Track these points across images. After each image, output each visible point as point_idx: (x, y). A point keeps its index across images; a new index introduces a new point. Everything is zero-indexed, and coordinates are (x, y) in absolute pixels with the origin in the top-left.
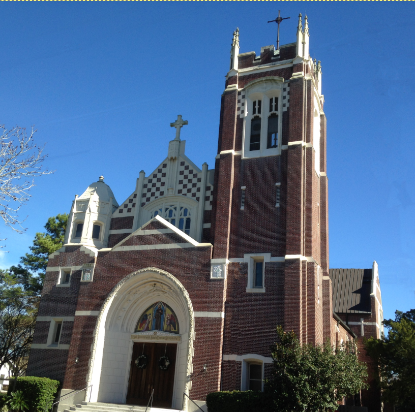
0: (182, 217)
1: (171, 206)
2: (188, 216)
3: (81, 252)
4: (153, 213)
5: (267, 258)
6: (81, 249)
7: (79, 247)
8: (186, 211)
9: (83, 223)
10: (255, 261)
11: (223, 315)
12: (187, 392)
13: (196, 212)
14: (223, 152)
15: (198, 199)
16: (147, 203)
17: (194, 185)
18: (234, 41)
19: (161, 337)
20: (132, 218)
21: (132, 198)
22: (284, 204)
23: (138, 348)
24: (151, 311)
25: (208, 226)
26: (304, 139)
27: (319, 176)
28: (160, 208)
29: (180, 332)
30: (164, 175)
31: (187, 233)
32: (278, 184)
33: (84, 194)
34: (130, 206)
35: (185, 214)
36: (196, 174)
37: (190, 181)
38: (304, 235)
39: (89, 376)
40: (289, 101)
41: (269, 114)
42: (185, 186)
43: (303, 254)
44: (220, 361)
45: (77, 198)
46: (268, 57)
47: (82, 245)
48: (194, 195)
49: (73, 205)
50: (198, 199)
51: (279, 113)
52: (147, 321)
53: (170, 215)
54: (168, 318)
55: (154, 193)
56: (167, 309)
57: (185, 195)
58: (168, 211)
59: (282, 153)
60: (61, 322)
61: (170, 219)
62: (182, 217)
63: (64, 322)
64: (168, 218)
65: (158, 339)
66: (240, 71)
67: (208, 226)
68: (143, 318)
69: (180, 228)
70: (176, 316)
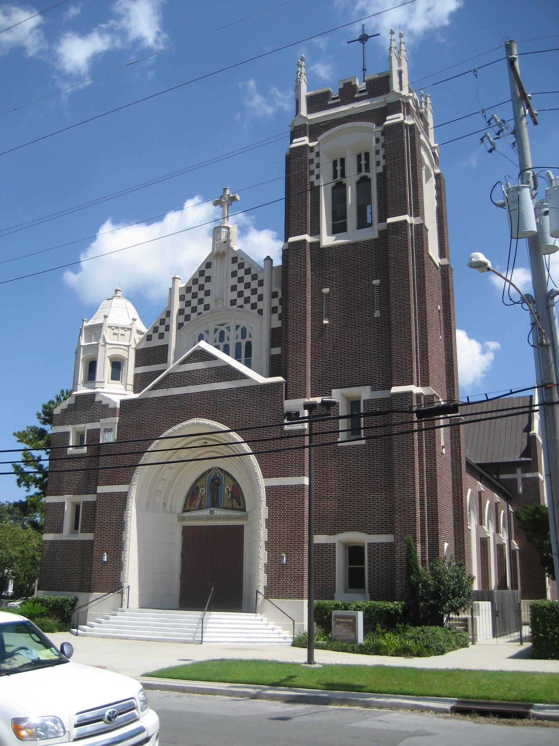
0: (240, 340)
1: (222, 325)
2: (248, 339)
3: (97, 402)
4: (197, 338)
5: (365, 393)
6: (97, 399)
7: (93, 395)
8: (244, 331)
9: (97, 359)
10: (348, 398)
11: (306, 481)
12: (262, 590)
13: (260, 333)
14: (291, 240)
15: (260, 312)
16: (186, 323)
17: (254, 292)
18: (299, 73)
19: (221, 517)
20: (165, 348)
21: (164, 317)
22: (386, 313)
23: (187, 532)
24: (202, 482)
25: (277, 351)
26: (411, 212)
27: (438, 266)
28: (206, 329)
29: (247, 509)
30: (208, 279)
31: (248, 364)
32: (376, 282)
33: (95, 317)
34: (162, 329)
35: (244, 336)
36: (256, 275)
37: (247, 286)
38: (417, 356)
39: (124, 574)
40: (384, 157)
41: (357, 178)
42: (240, 294)
43: (418, 383)
44: (306, 546)
45: (85, 324)
46: (348, 93)
47: (98, 392)
48: (254, 306)
49: (81, 334)
50: (260, 312)
51: (373, 176)
52: (199, 496)
53: (222, 338)
54: (228, 489)
55: (193, 298)
56: (227, 477)
57: (241, 306)
58: (218, 333)
59: (379, 235)
60: (80, 502)
61: (222, 345)
62: (240, 340)
63: (84, 503)
64: (218, 343)
65: (216, 521)
66: (310, 117)
67: (277, 351)
68: (193, 492)
69: (237, 357)
70: (239, 486)
